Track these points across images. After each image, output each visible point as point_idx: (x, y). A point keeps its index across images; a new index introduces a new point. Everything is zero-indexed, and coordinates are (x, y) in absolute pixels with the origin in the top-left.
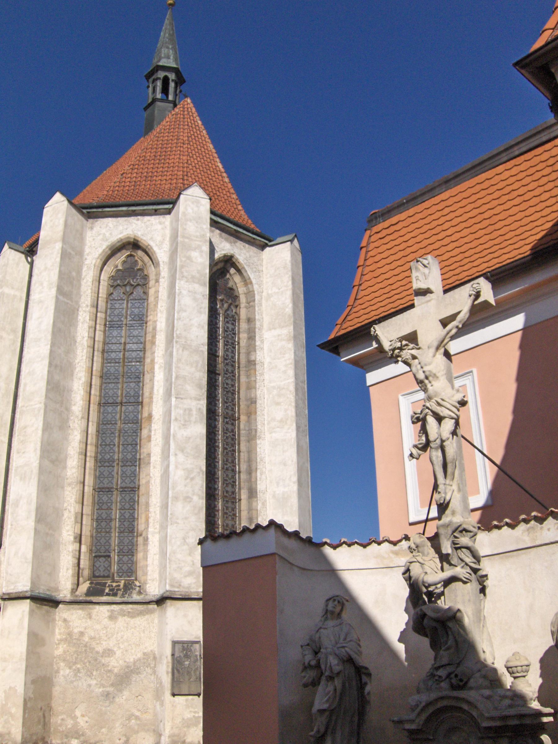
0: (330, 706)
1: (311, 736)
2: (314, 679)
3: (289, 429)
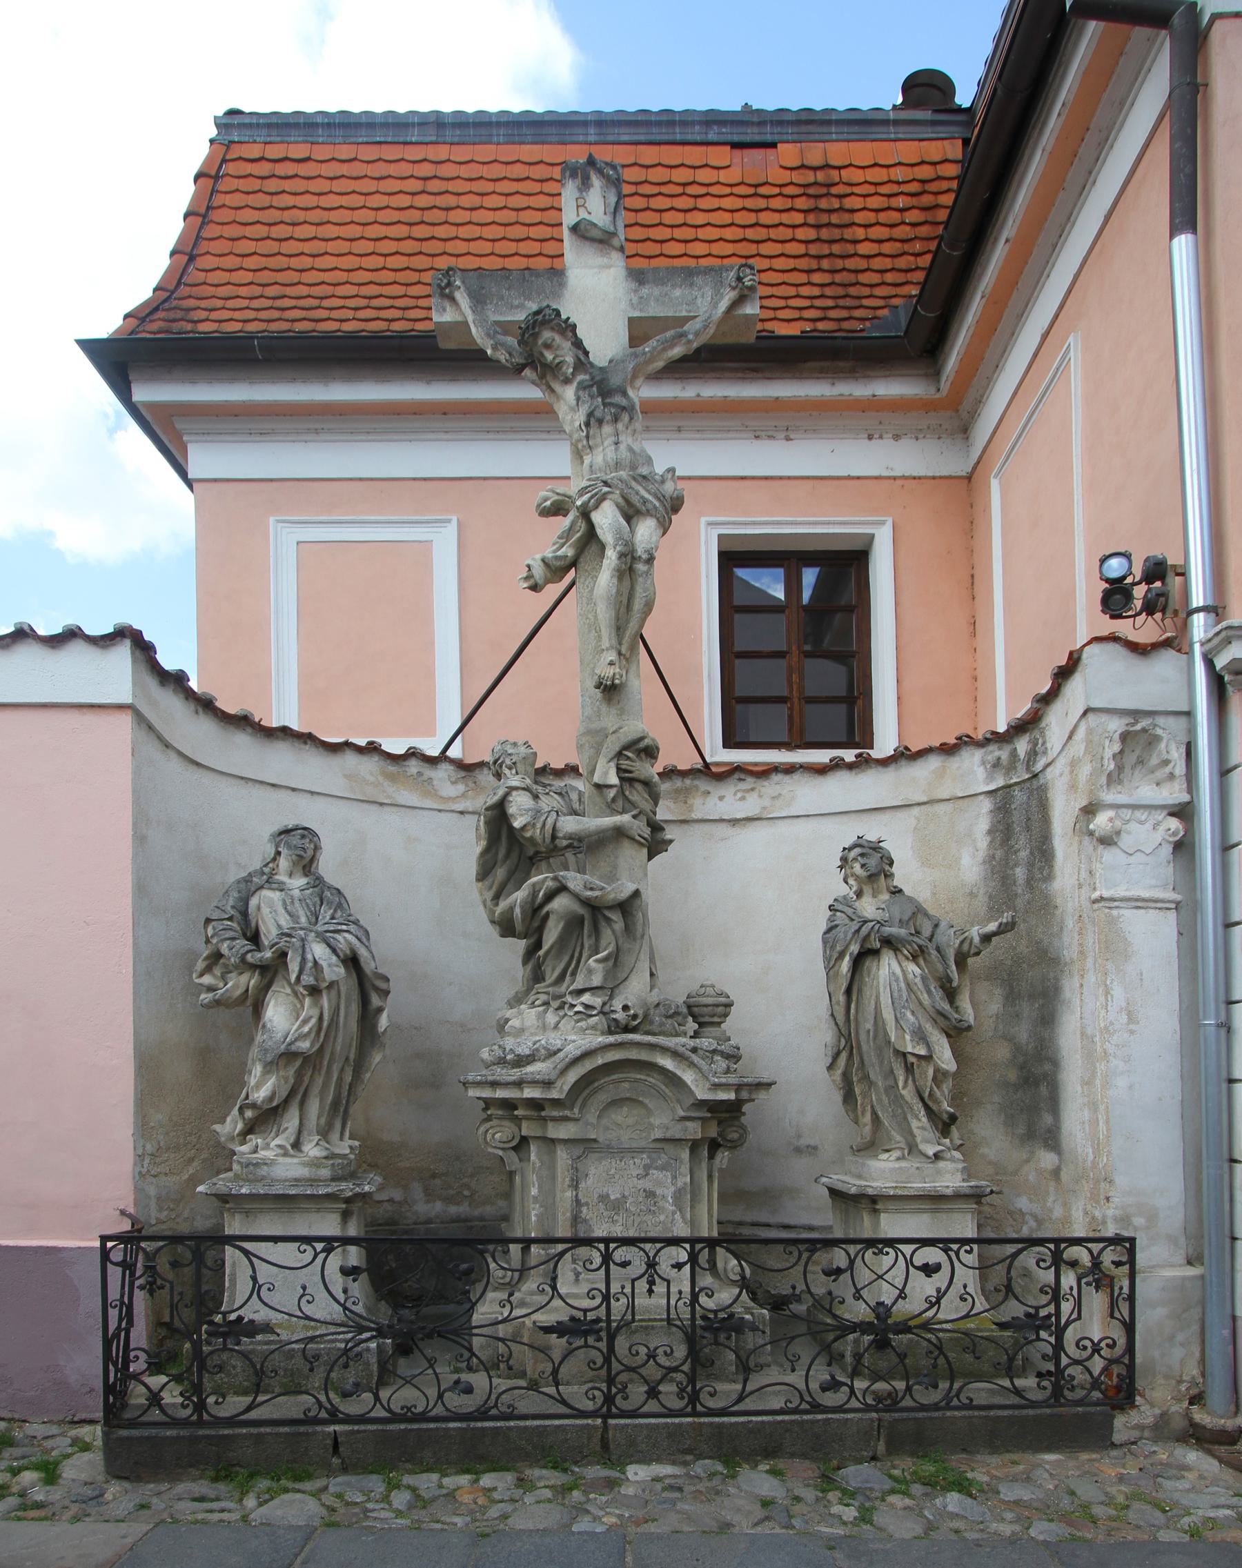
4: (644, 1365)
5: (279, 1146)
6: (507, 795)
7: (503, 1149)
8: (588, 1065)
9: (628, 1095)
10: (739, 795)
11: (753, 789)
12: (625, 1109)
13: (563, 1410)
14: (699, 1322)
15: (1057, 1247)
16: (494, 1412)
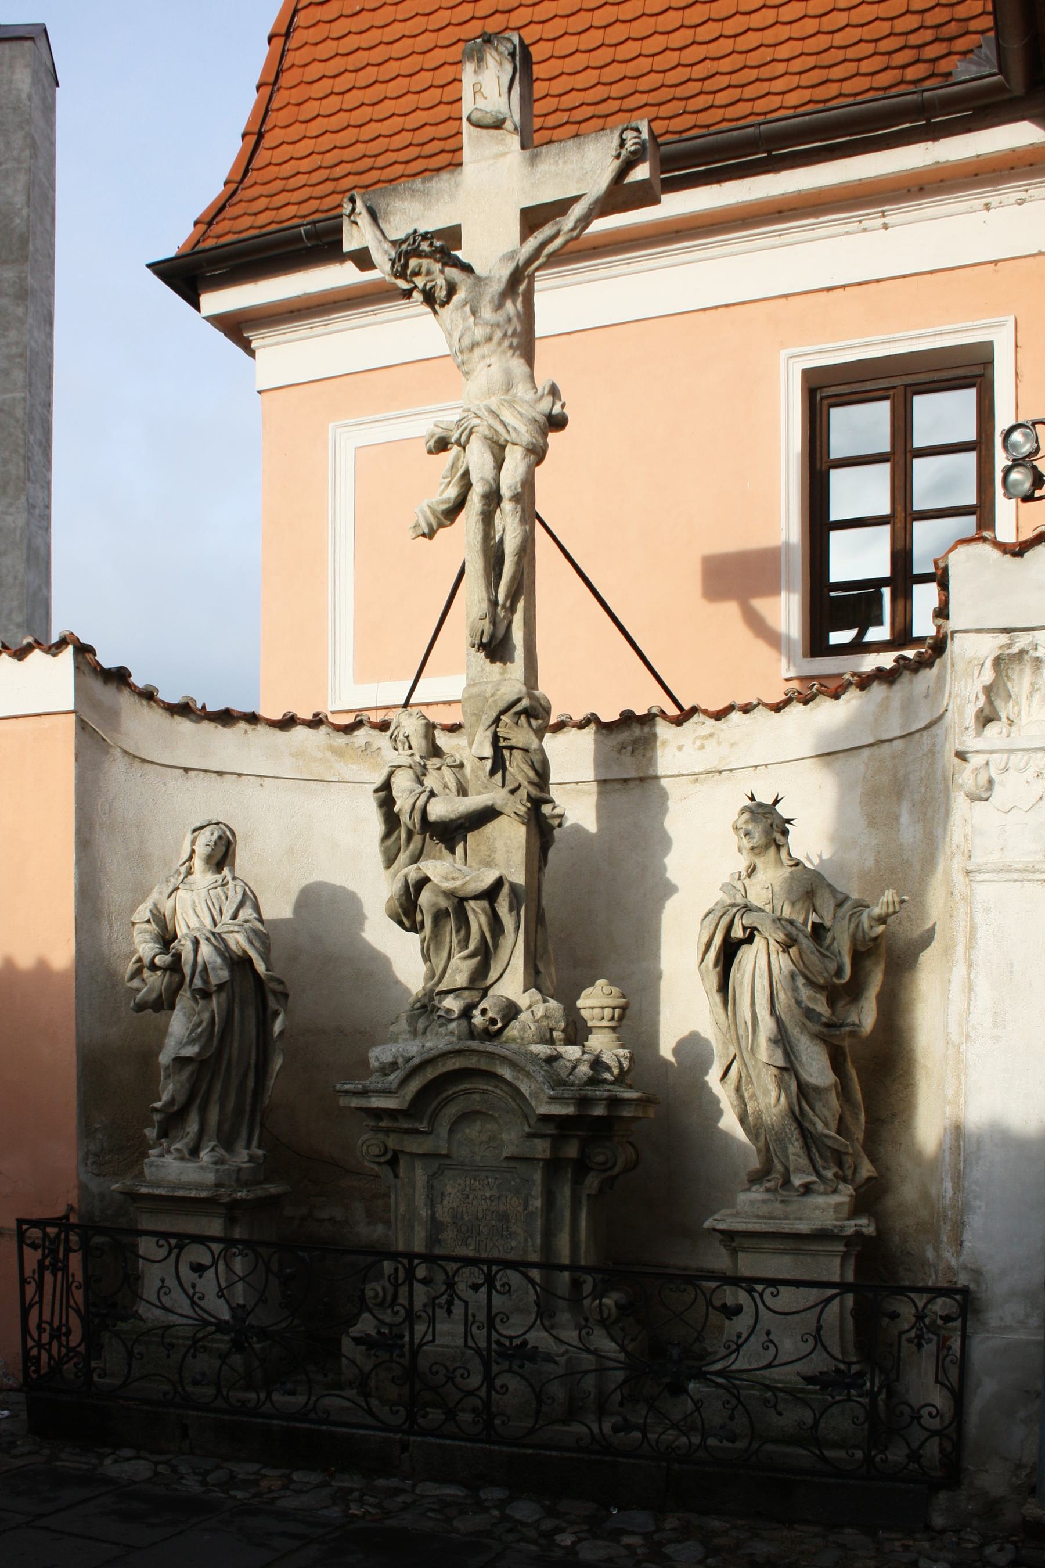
0: (203, 1049)
1: (156, 1110)
2: (161, 995)
3: (10, 505)
4: (443, 1386)
5: (177, 1150)
6: (390, 775)
7: (379, 1163)
8: (430, 1074)
9: (478, 1108)
10: (698, 743)
11: (711, 735)
12: (479, 1123)
13: (369, 1421)
14: (494, 1346)
15: (411, 1263)
16: (312, 1415)
